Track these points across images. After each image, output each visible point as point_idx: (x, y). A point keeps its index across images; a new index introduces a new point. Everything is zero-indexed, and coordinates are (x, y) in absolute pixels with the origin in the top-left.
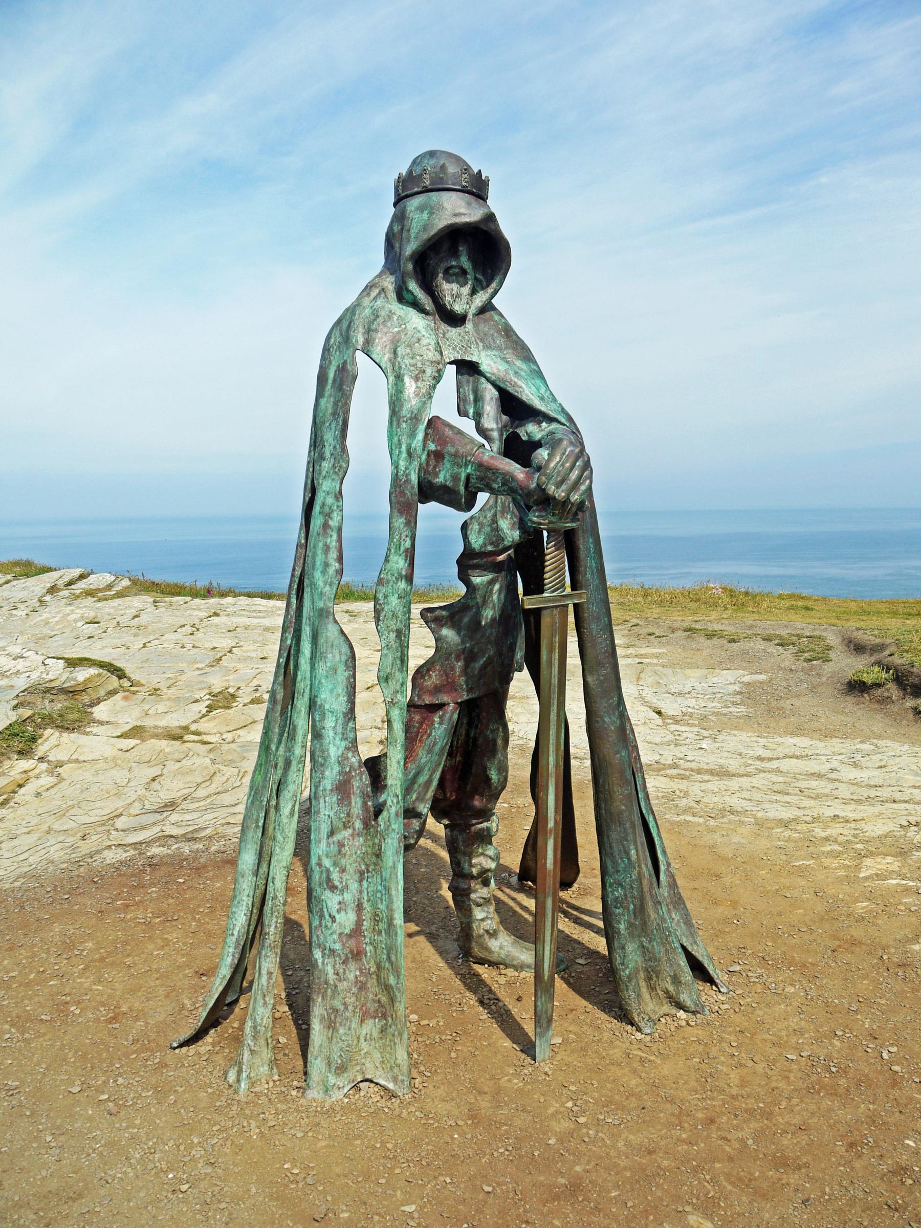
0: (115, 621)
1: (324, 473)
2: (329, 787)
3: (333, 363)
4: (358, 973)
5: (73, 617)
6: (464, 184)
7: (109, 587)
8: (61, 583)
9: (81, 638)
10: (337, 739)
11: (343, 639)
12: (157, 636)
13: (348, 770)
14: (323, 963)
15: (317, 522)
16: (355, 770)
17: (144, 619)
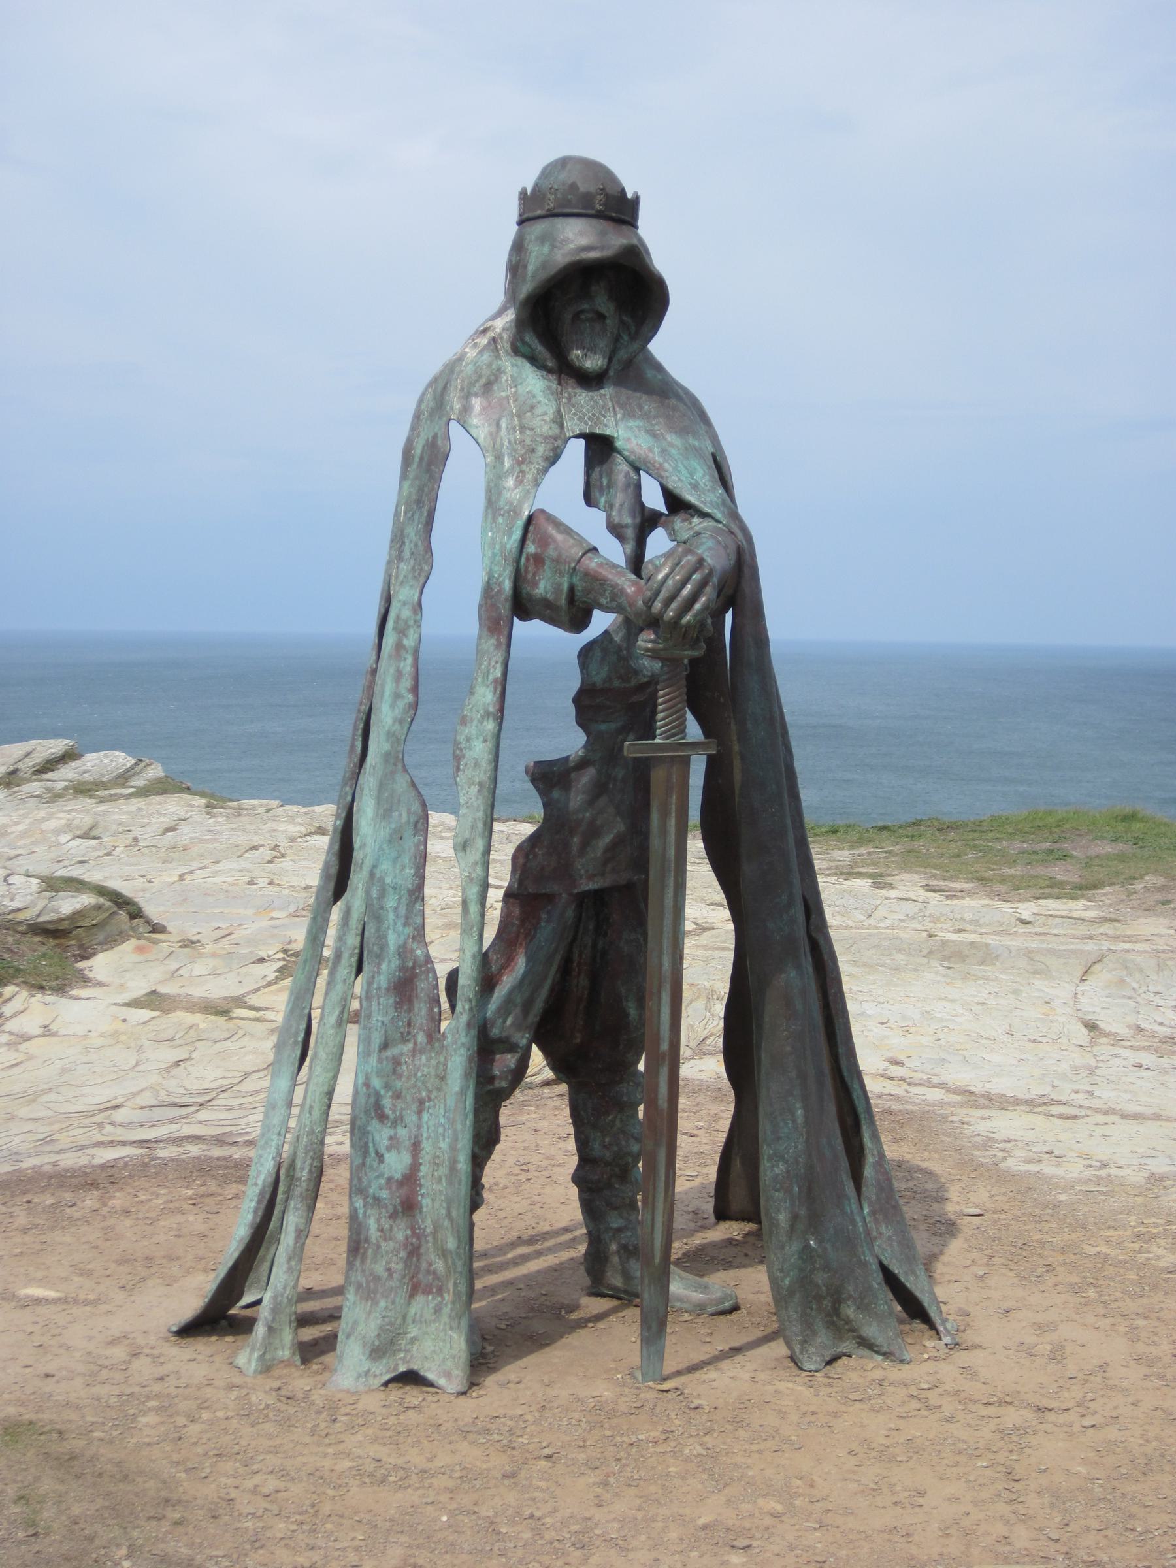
0: (130, 836)
1: (401, 577)
2: (384, 985)
3: (422, 434)
4: (409, 1233)
5: (52, 824)
6: (598, 207)
7: (123, 778)
8: (26, 766)
9: (66, 863)
10: (399, 924)
11: (414, 793)
12: (206, 862)
13: (410, 964)
14: (365, 1213)
15: (390, 639)
16: (421, 967)
17: (185, 832)
